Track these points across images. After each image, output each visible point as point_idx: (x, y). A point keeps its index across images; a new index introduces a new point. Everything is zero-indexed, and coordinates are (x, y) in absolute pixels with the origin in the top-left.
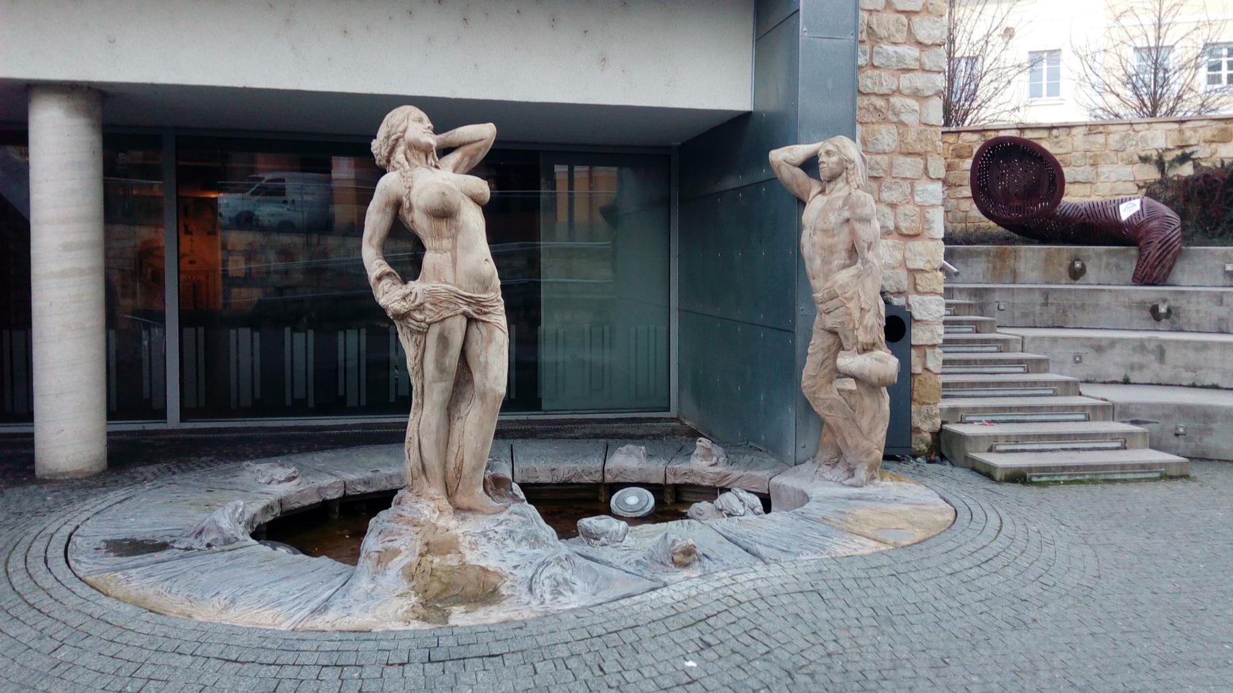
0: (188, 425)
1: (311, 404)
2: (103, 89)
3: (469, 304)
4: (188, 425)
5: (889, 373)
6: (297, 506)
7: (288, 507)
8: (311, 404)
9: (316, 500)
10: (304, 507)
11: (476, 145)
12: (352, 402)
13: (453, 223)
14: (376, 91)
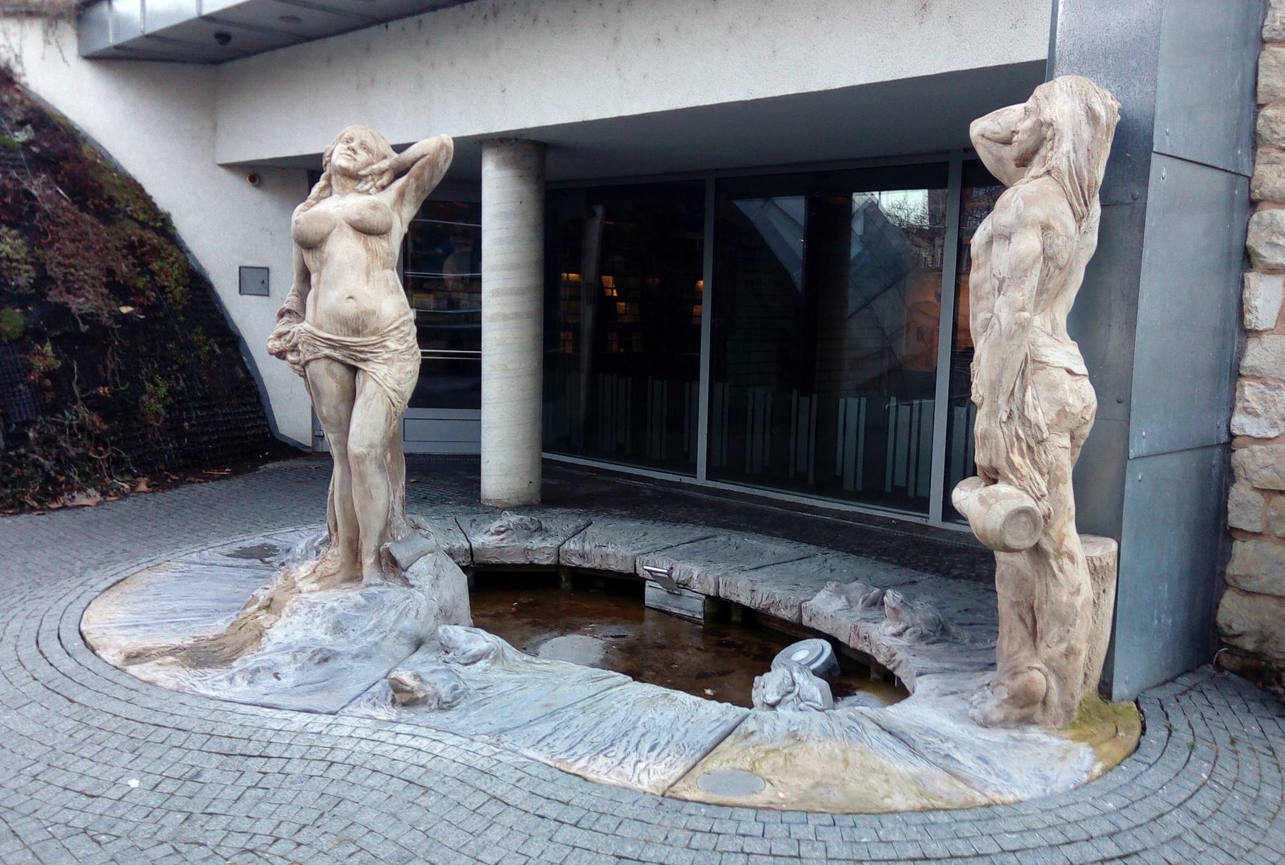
0: (711, 484)
1: (811, 481)
2: (543, 138)
3: (333, 347)
4: (711, 484)
5: (989, 526)
6: (494, 561)
7: (1268, 647)
8: (811, 481)
9: (521, 560)
10: (504, 565)
11: (419, 163)
12: (848, 485)
13: (318, 254)
14: (725, 100)
